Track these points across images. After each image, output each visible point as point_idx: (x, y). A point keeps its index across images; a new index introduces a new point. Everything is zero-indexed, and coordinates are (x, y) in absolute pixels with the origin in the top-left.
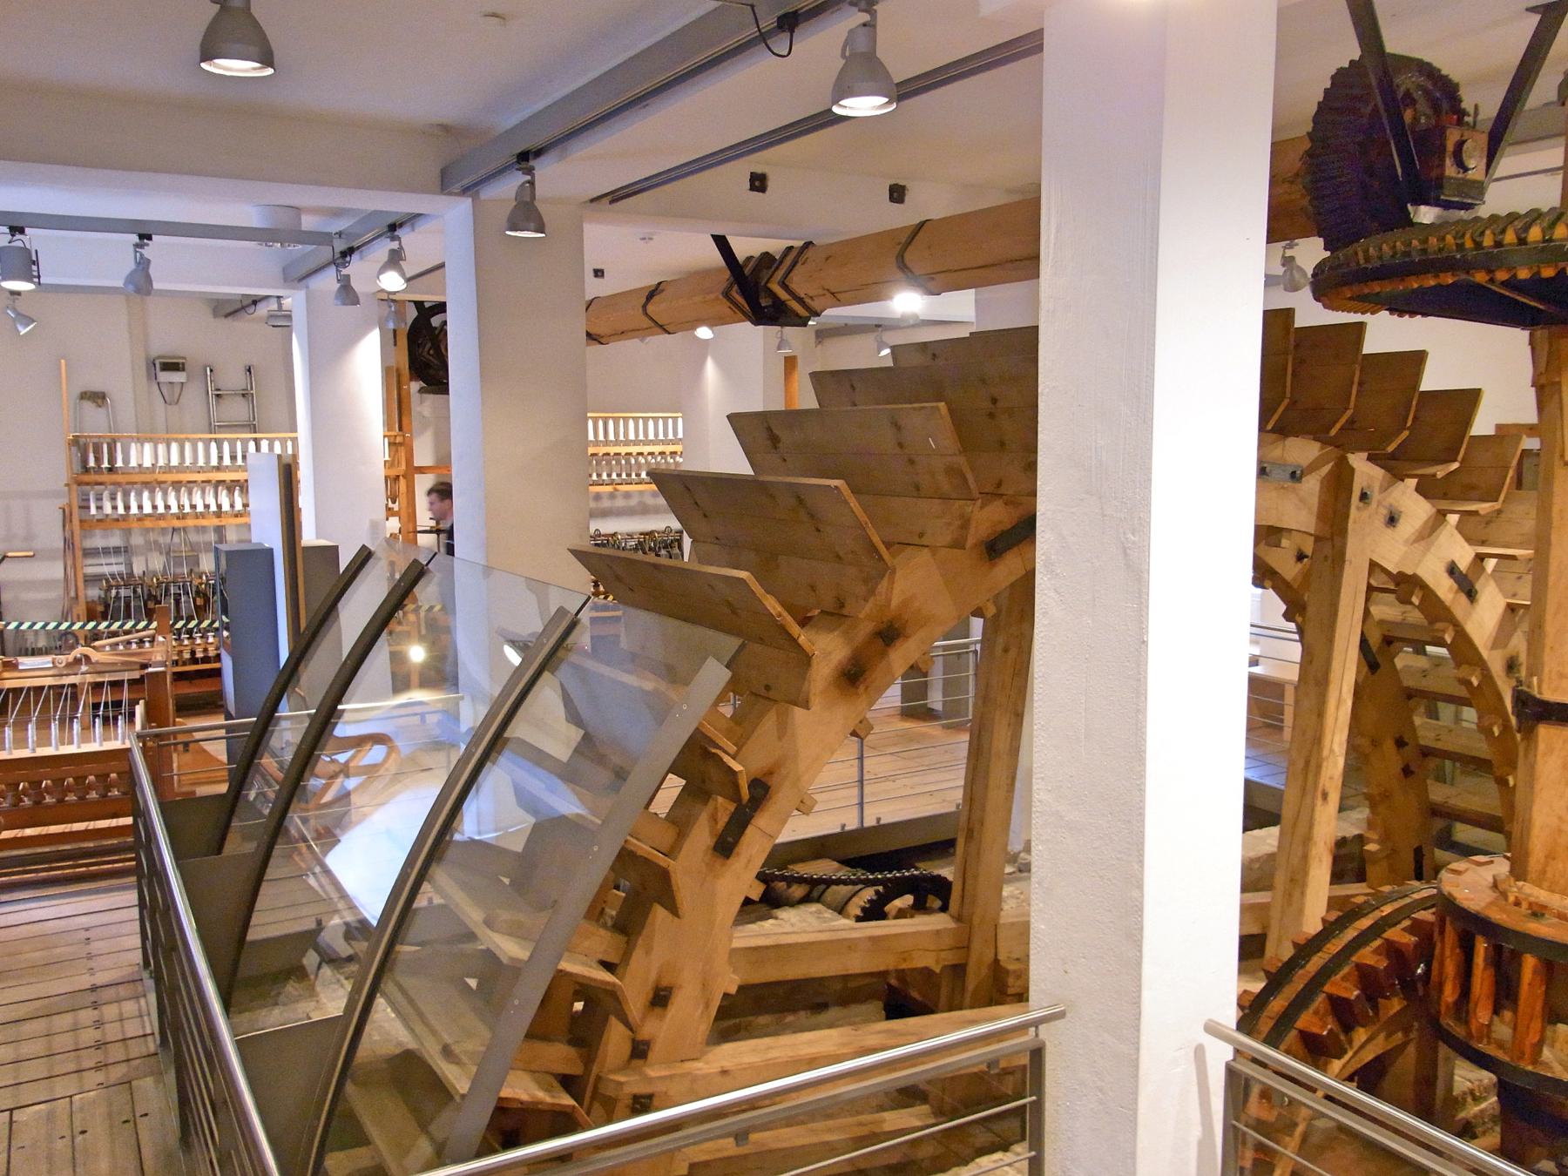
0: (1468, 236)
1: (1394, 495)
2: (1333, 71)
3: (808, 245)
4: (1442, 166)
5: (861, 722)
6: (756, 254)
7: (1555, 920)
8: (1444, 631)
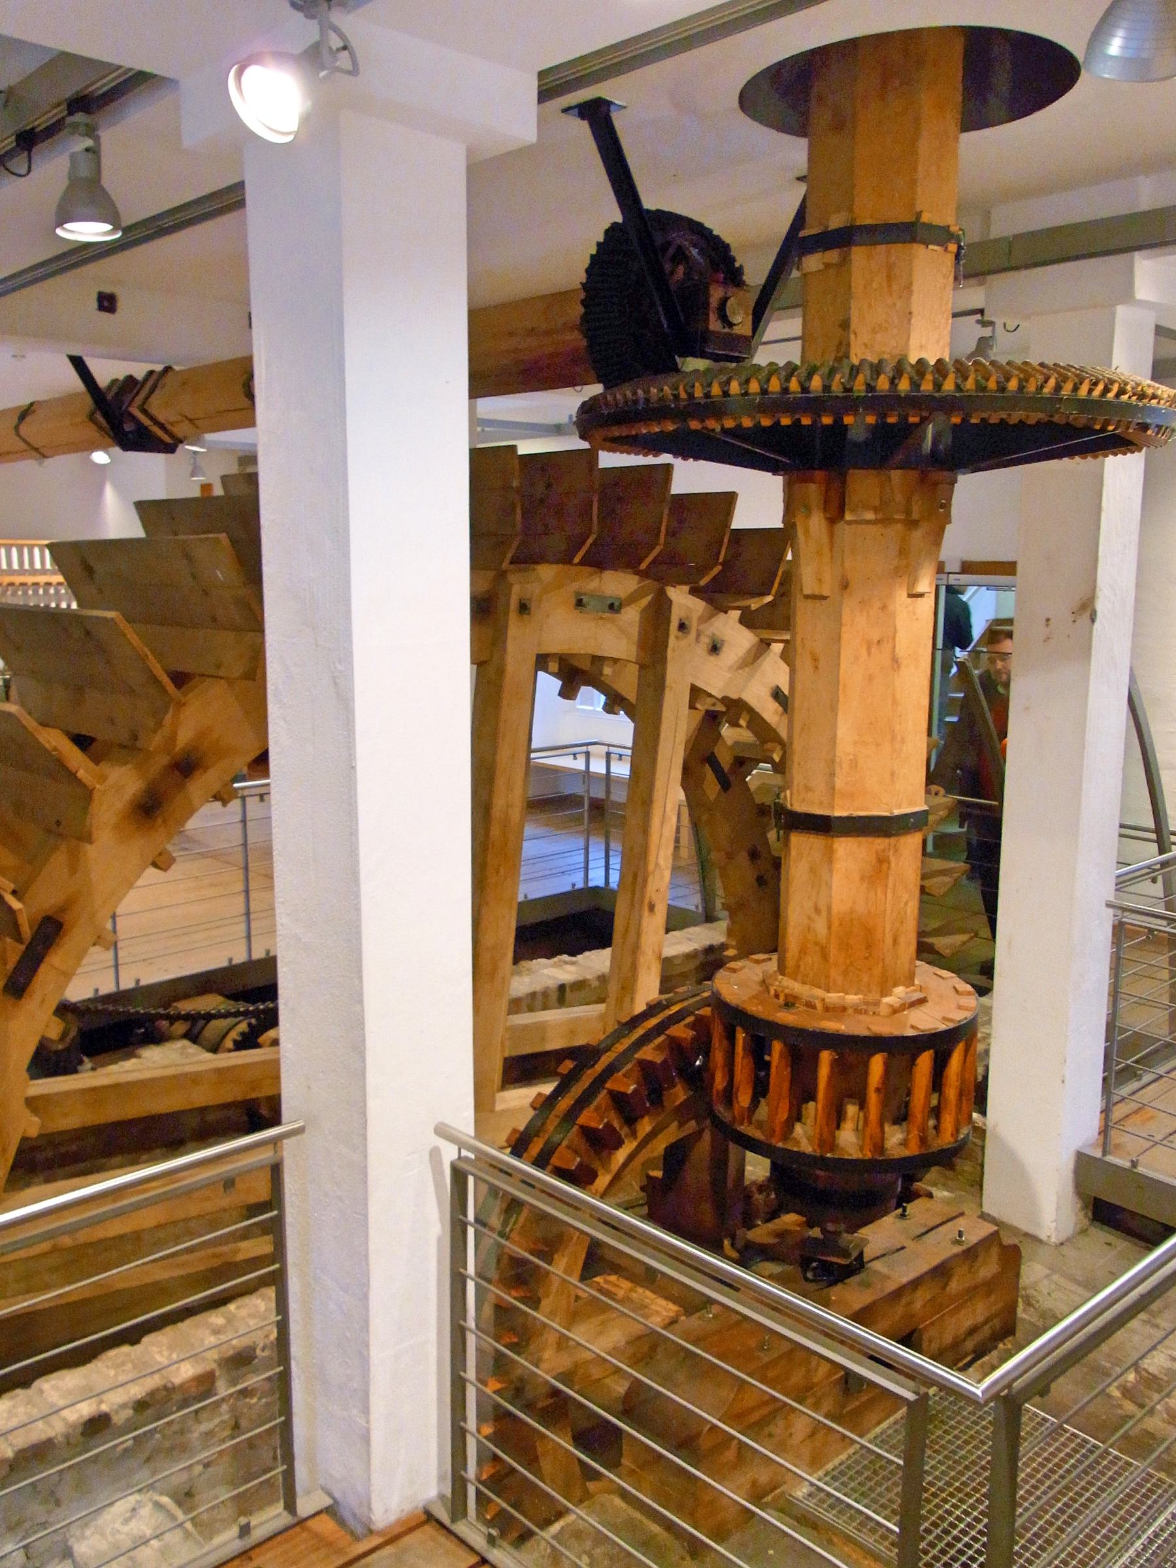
0: (681, 388)
1: (716, 624)
2: (607, 226)
3: (168, 369)
4: (707, 320)
5: (160, 854)
6: (121, 377)
7: (802, 1008)
8: (772, 751)
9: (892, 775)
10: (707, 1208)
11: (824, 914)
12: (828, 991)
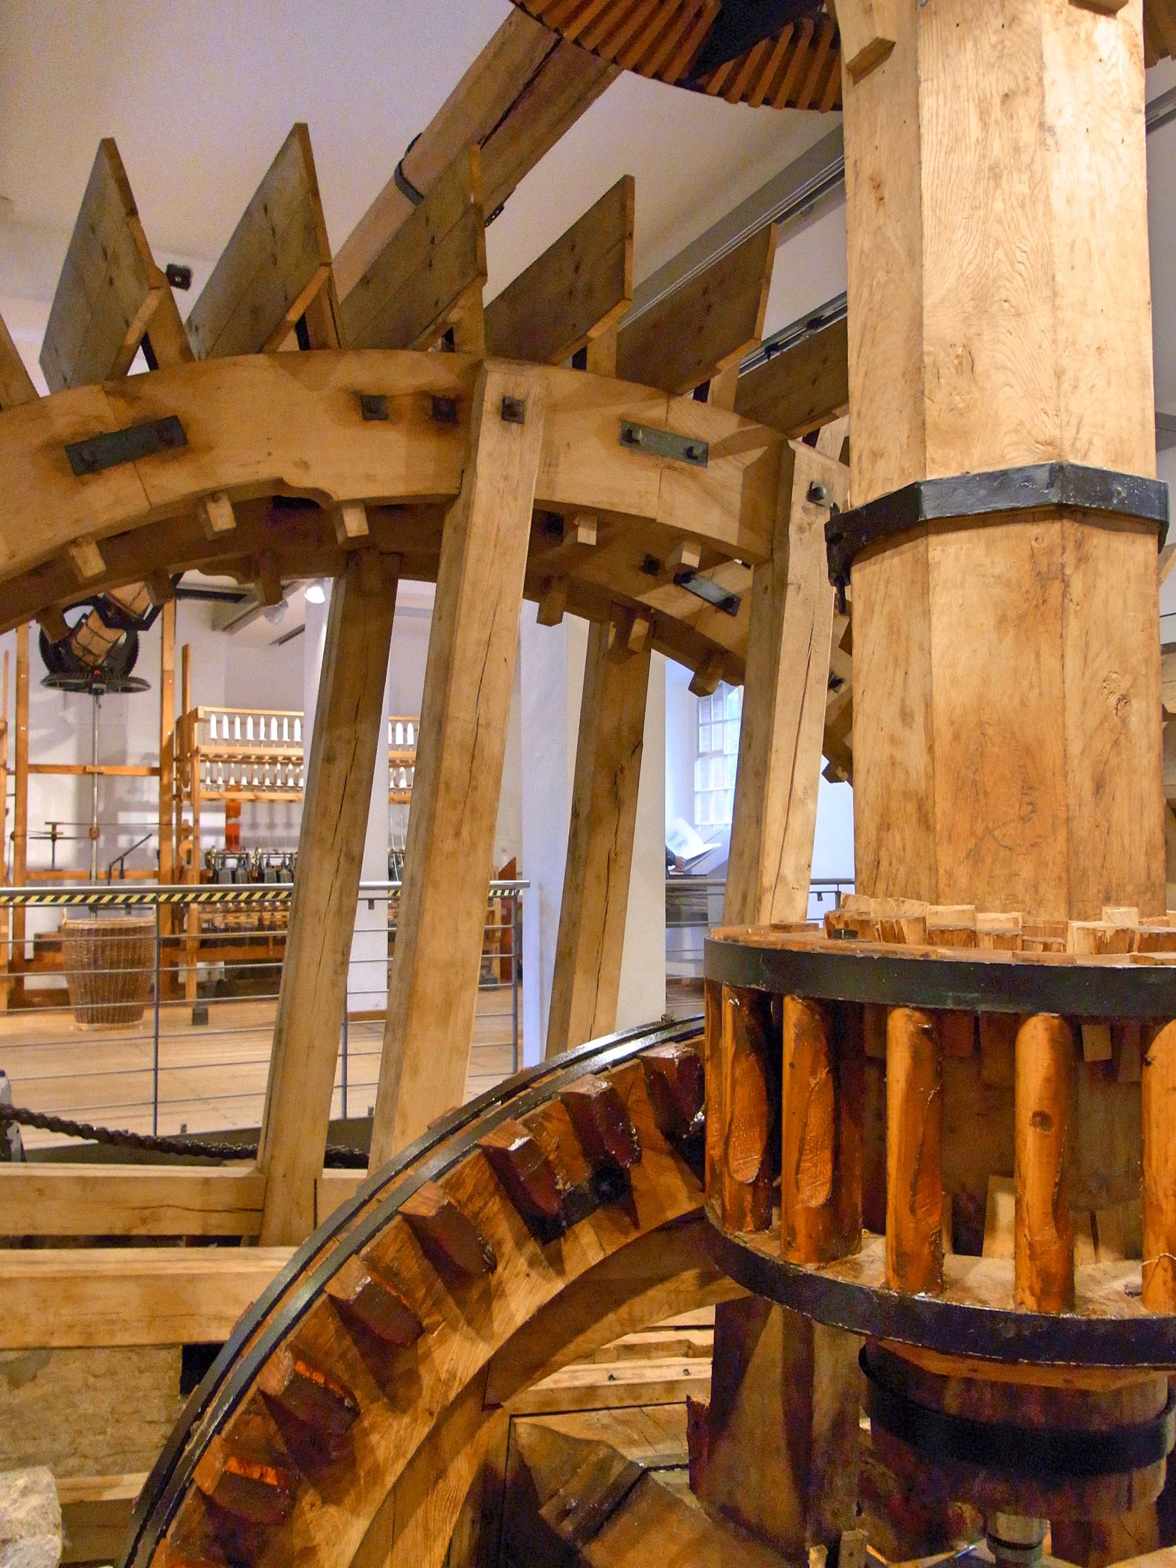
9: (1059, 374)
10: (779, 1472)
11: (919, 719)
12: (936, 902)
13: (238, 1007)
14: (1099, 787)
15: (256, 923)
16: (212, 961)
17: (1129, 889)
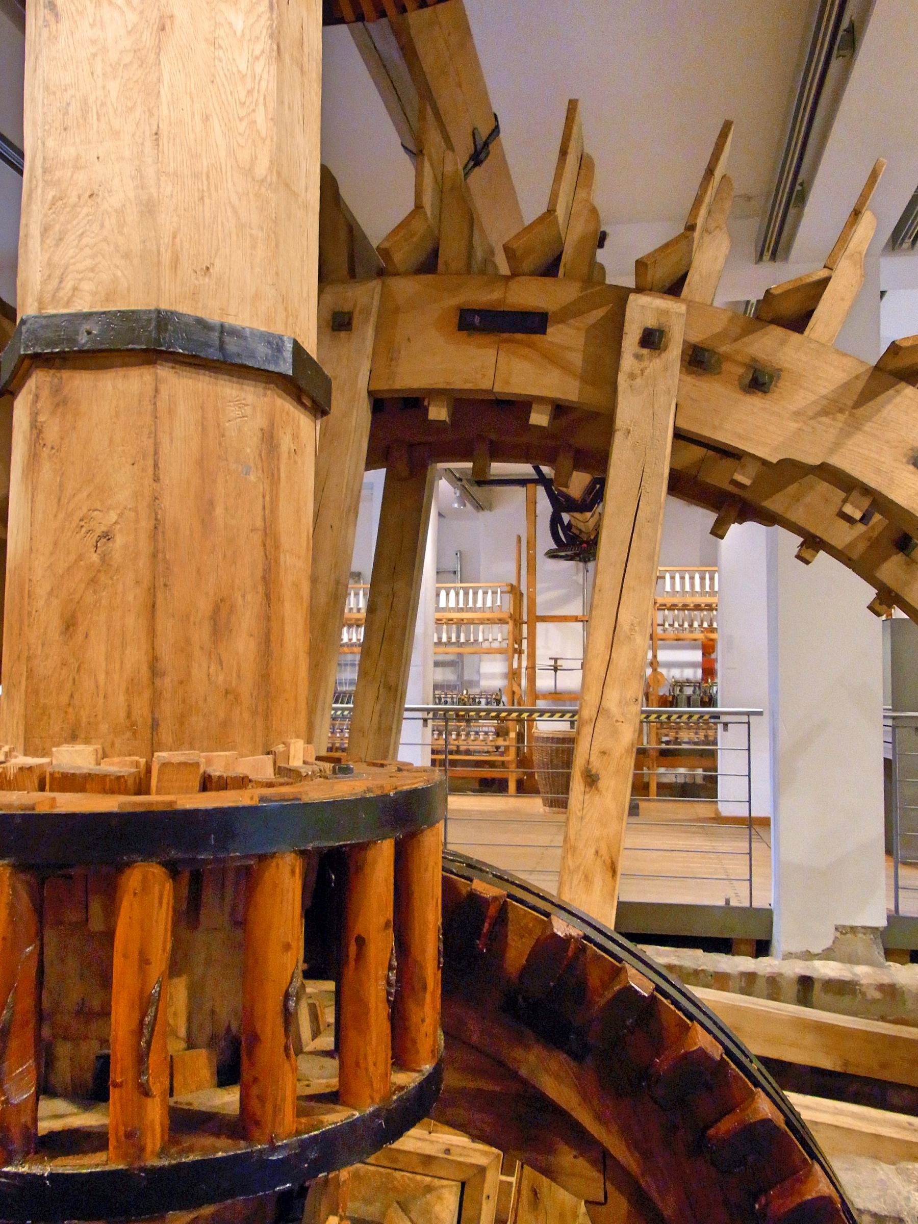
13: (689, 805)
14: (69, 625)
15: (703, 738)
16: (692, 767)
17: (104, 728)
